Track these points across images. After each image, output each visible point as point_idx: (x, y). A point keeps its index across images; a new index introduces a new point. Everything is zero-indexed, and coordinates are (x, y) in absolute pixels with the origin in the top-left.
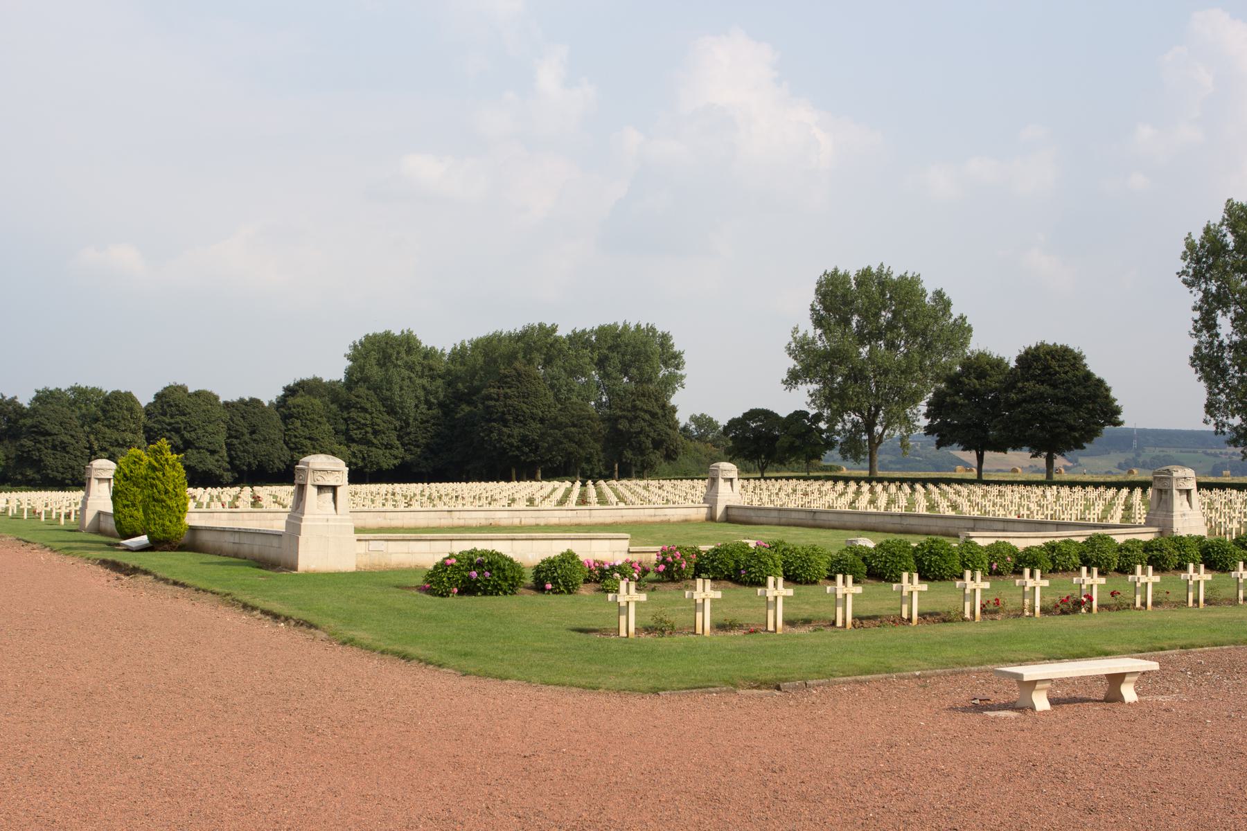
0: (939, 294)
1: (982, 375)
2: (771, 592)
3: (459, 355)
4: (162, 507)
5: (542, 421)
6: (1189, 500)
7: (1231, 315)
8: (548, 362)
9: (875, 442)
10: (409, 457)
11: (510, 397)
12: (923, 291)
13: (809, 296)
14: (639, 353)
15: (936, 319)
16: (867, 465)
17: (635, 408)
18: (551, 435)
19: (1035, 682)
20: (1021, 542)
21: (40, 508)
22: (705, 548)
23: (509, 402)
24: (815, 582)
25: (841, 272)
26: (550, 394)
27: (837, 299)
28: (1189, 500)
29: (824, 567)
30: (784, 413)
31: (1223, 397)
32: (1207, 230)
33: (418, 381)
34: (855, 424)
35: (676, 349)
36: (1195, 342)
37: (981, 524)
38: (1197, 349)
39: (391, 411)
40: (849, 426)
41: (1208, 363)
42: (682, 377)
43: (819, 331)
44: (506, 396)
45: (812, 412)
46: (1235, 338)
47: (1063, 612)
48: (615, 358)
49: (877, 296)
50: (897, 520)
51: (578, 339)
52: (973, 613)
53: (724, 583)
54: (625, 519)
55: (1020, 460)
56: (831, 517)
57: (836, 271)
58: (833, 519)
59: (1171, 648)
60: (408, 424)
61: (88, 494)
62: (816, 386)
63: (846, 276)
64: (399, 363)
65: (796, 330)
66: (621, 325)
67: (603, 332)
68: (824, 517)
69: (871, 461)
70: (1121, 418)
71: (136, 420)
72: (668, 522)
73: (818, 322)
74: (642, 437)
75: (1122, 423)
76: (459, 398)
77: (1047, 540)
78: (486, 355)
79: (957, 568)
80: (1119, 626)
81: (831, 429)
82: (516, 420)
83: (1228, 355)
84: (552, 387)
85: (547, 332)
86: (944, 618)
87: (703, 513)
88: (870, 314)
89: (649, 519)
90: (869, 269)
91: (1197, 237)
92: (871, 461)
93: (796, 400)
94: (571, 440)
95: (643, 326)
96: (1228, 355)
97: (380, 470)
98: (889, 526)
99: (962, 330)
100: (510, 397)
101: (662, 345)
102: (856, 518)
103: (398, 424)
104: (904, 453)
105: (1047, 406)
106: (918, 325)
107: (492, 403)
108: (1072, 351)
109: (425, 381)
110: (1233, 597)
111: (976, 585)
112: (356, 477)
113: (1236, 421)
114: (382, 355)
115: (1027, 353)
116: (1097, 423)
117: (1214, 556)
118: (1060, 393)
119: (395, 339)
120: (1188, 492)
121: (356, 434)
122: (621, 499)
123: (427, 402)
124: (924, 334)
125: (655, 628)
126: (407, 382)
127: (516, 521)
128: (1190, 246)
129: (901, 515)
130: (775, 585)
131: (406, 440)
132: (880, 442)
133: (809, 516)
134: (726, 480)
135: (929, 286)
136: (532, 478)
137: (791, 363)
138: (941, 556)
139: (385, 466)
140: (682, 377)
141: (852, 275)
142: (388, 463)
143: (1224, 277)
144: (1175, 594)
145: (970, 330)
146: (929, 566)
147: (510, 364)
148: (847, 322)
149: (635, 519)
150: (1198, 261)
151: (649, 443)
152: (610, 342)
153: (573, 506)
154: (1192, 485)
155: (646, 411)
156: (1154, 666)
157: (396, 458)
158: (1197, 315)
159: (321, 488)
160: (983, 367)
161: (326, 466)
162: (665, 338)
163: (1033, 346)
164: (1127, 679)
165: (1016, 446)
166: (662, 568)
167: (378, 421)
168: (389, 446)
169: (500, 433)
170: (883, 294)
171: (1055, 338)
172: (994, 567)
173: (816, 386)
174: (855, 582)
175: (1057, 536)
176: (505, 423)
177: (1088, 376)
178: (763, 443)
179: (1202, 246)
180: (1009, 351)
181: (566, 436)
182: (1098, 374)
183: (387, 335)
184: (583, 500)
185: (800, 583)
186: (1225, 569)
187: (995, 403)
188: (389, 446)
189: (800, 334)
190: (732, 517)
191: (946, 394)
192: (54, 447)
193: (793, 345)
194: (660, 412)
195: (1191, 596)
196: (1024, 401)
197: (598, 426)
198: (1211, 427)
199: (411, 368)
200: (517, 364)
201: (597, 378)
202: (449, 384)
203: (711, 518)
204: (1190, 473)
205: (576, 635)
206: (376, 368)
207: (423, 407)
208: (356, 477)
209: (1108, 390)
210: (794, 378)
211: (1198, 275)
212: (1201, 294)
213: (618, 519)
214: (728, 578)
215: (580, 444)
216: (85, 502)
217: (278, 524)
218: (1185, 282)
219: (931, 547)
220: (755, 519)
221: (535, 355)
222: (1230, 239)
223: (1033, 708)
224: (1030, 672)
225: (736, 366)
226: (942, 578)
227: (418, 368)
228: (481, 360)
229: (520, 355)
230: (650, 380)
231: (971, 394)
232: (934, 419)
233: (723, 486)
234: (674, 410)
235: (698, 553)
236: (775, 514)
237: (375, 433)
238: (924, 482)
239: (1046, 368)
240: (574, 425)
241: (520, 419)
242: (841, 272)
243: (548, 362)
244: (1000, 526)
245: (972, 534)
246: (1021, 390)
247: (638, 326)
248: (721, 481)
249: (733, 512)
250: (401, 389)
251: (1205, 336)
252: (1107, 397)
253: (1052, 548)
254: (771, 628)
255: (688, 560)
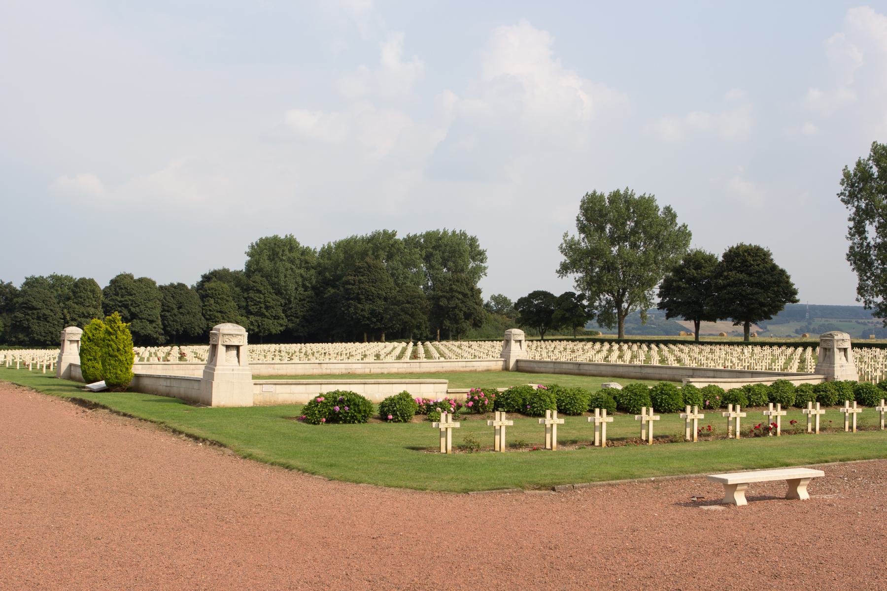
0: (668, 209)
1: (698, 267)
2: (548, 421)
3: (326, 252)
4: (116, 361)
5: (385, 299)
6: (846, 355)
7: (876, 224)
8: (390, 257)
9: (622, 314)
10: (291, 325)
11: (363, 283)
12: (657, 207)
13: (575, 211)
14: (454, 251)
15: (666, 227)
16: (617, 331)
17: (451, 290)
18: (392, 309)
19: (736, 485)
20: (726, 385)
21: (29, 361)
22: (501, 389)
23: (362, 286)
24: (580, 414)
25: (598, 193)
26: (391, 280)
27: (595, 212)
28: (846, 355)
29: (586, 403)
30: (557, 294)
31: (870, 282)
32: (859, 164)
33: (298, 271)
34: (608, 302)
35: (481, 248)
36: (850, 243)
37: (698, 373)
38: (852, 248)
39: (278, 292)
40: (604, 303)
41: (859, 259)
42: (485, 268)
43: (582, 236)
44: (360, 282)
45: (578, 293)
46: (879, 240)
47: (756, 436)
48: (438, 255)
49: (623, 210)
50: (638, 370)
51: (411, 241)
52: (692, 436)
53: (515, 415)
54: (444, 369)
55: (725, 327)
56: (591, 368)
57: (595, 192)
58: (593, 369)
59: (833, 461)
60: (290, 302)
61: (62, 351)
62: (580, 275)
63: (602, 196)
64: (284, 258)
65: (566, 235)
66: (442, 231)
67: (429, 236)
68: (586, 367)
69: (620, 328)
70: (797, 297)
71: (97, 299)
72: (475, 372)
73: (582, 229)
74: (457, 311)
75: (798, 301)
76: (327, 283)
77: (745, 384)
78: (346, 252)
79: (681, 404)
80: (796, 445)
81: (591, 305)
82: (367, 299)
83: (873, 253)
84: (393, 275)
85: (389, 236)
86: (672, 440)
87: (500, 365)
88: (618, 224)
89: (462, 369)
90: (618, 191)
91: (852, 168)
92: (620, 328)
93: (566, 285)
94: (406, 313)
95: (458, 232)
96: (873, 253)
97: (270, 334)
98: (633, 374)
99: (684, 235)
100: (363, 283)
101: (471, 245)
102: (609, 369)
103: (283, 301)
104: (643, 322)
105: (745, 288)
106: (653, 231)
107: (350, 287)
108: (762, 250)
109: (302, 271)
110: (877, 424)
111: (694, 416)
112: (253, 339)
113: (879, 299)
114: (272, 253)
115: (730, 251)
116: (780, 301)
117: (864, 396)
118: (754, 279)
119: (281, 241)
120: (845, 350)
121: (253, 309)
122: (442, 355)
123: (304, 286)
124: (657, 238)
125: (466, 446)
126: (289, 272)
127: (367, 371)
128: (847, 175)
129: (641, 367)
130: (551, 416)
131: (289, 313)
132: (626, 314)
133: (576, 367)
134: (516, 341)
135: (661, 204)
136: (378, 340)
137: (563, 258)
138: (669, 395)
139: (274, 332)
140: (485, 268)
141: (606, 195)
142: (276, 329)
143: (870, 197)
144: (836, 422)
145: (690, 234)
146: (661, 402)
147: (363, 259)
148: (603, 229)
149: (451, 369)
150: (852, 186)
151: (461, 315)
152: (434, 243)
153: (408, 360)
154: (848, 345)
155: (459, 293)
156: (821, 474)
157: (282, 326)
158: (851, 224)
159: (228, 347)
160: (699, 261)
161: (232, 332)
162: (473, 240)
163: (735, 246)
164: (802, 483)
165: (723, 317)
166: (471, 404)
167: (269, 299)
168: (276, 317)
169: (356, 308)
170: (628, 209)
171: (750, 240)
172: (707, 403)
173: (580, 275)
174: (608, 414)
175: (752, 382)
176: (359, 301)
177: (774, 267)
178: (543, 315)
179: (855, 175)
180: (717, 250)
181: (402, 310)
182: (781, 266)
183: (275, 238)
184: (415, 356)
185: (569, 414)
186: (871, 405)
187: (708, 287)
188: (276, 317)
189: (569, 238)
190: (521, 368)
191: (673, 281)
192: (39, 318)
193: (564, 245)
194: (469, 293)
195: (847, 424)
196: (729, 285)
197: (426, 303)
198: (862, 304)
199: (292, 262)
200: (368, 259)
201: (424, 269)
202: (320, 273)
203: (506, 369)
204: (846, 336)
205: (410, 451)
206: (267, 261)
207: (301, 289)
208: (253, 339)
209: (788, 277)
210: (565, 269)
211: (852, 195)
212: (854, 209)
213: (440, 369)
214: (518, 411)
215: (412, 315)
216: (60, 357)
217: (198, 373)
218: (843, 200)
219: (662, 389)
220: (537, 369)
221: (381, 252)
222: (875, 170)
223: (735, 504)
224: (733, 478)
225: (523, 260)
226: (670, 411)
227: (298, 262)
228: (342, 256)
229: (370, 253)
230: (462, 270)
231: (691, 280)
232: (664, 298)
233: (514, 346)
234: (479, 291)
235: (497, 393)
236: (551, 365)
237: (267, 308)
238: (657, 343)
239: (744, 261)
240: (408, 303)
241: (370, 298)
242: (598, 193)
243: (390, 257)
244: (712, 374)
245: (691, 380)
246: (726, 278)
247: (454, 232)
248: (513, 342)
249: (521, 364)
250: (285, 276)
251: (857, 239)
252: (788, 282)
253: (748, 389)
254: (548, 446)
255: (489, 398)
